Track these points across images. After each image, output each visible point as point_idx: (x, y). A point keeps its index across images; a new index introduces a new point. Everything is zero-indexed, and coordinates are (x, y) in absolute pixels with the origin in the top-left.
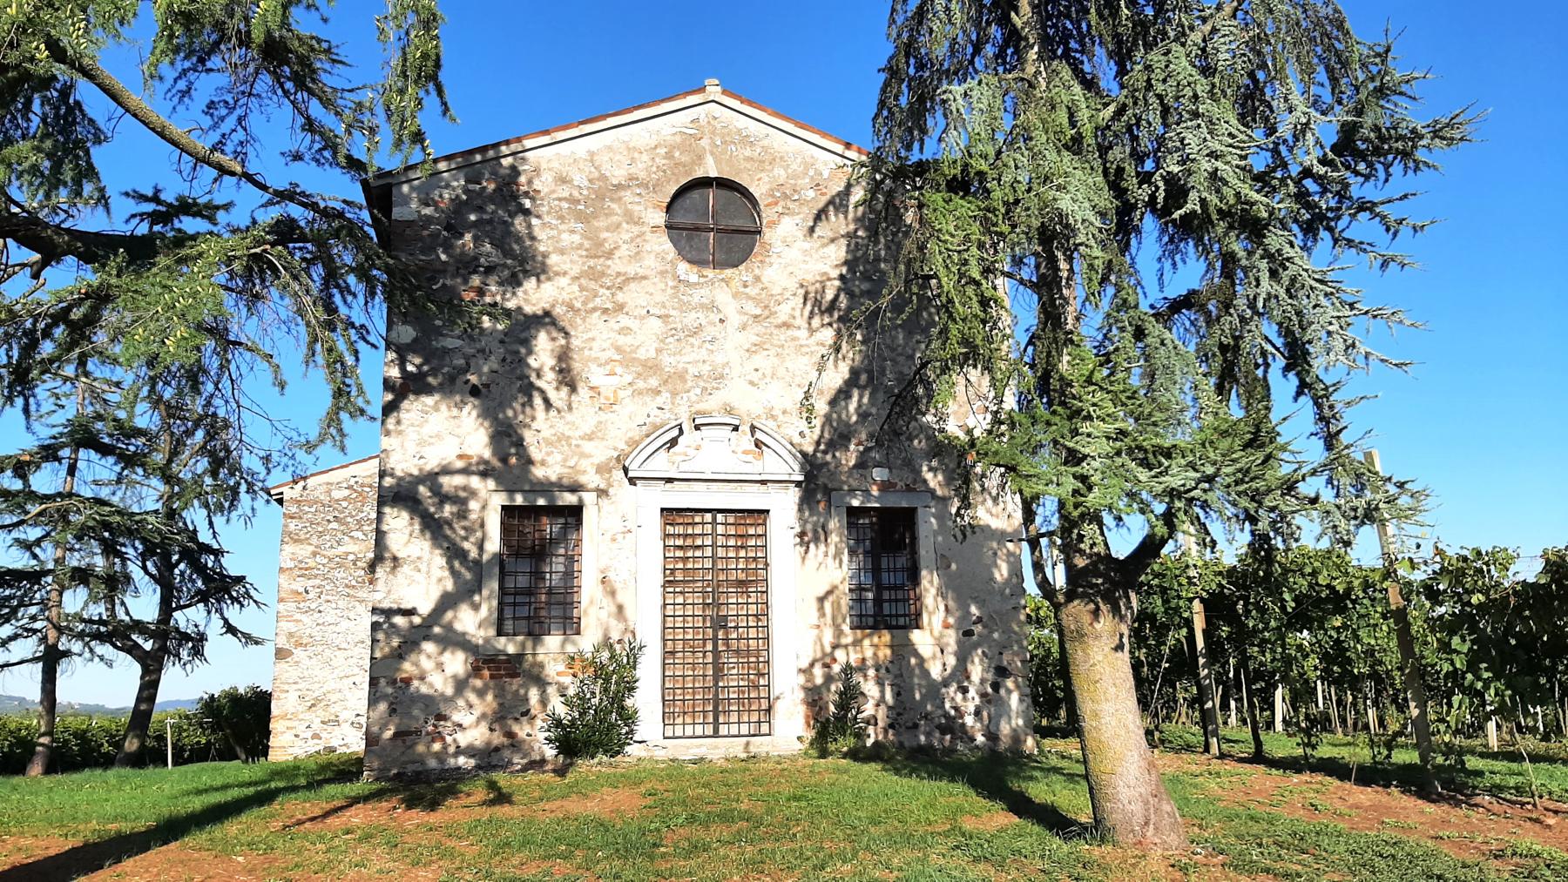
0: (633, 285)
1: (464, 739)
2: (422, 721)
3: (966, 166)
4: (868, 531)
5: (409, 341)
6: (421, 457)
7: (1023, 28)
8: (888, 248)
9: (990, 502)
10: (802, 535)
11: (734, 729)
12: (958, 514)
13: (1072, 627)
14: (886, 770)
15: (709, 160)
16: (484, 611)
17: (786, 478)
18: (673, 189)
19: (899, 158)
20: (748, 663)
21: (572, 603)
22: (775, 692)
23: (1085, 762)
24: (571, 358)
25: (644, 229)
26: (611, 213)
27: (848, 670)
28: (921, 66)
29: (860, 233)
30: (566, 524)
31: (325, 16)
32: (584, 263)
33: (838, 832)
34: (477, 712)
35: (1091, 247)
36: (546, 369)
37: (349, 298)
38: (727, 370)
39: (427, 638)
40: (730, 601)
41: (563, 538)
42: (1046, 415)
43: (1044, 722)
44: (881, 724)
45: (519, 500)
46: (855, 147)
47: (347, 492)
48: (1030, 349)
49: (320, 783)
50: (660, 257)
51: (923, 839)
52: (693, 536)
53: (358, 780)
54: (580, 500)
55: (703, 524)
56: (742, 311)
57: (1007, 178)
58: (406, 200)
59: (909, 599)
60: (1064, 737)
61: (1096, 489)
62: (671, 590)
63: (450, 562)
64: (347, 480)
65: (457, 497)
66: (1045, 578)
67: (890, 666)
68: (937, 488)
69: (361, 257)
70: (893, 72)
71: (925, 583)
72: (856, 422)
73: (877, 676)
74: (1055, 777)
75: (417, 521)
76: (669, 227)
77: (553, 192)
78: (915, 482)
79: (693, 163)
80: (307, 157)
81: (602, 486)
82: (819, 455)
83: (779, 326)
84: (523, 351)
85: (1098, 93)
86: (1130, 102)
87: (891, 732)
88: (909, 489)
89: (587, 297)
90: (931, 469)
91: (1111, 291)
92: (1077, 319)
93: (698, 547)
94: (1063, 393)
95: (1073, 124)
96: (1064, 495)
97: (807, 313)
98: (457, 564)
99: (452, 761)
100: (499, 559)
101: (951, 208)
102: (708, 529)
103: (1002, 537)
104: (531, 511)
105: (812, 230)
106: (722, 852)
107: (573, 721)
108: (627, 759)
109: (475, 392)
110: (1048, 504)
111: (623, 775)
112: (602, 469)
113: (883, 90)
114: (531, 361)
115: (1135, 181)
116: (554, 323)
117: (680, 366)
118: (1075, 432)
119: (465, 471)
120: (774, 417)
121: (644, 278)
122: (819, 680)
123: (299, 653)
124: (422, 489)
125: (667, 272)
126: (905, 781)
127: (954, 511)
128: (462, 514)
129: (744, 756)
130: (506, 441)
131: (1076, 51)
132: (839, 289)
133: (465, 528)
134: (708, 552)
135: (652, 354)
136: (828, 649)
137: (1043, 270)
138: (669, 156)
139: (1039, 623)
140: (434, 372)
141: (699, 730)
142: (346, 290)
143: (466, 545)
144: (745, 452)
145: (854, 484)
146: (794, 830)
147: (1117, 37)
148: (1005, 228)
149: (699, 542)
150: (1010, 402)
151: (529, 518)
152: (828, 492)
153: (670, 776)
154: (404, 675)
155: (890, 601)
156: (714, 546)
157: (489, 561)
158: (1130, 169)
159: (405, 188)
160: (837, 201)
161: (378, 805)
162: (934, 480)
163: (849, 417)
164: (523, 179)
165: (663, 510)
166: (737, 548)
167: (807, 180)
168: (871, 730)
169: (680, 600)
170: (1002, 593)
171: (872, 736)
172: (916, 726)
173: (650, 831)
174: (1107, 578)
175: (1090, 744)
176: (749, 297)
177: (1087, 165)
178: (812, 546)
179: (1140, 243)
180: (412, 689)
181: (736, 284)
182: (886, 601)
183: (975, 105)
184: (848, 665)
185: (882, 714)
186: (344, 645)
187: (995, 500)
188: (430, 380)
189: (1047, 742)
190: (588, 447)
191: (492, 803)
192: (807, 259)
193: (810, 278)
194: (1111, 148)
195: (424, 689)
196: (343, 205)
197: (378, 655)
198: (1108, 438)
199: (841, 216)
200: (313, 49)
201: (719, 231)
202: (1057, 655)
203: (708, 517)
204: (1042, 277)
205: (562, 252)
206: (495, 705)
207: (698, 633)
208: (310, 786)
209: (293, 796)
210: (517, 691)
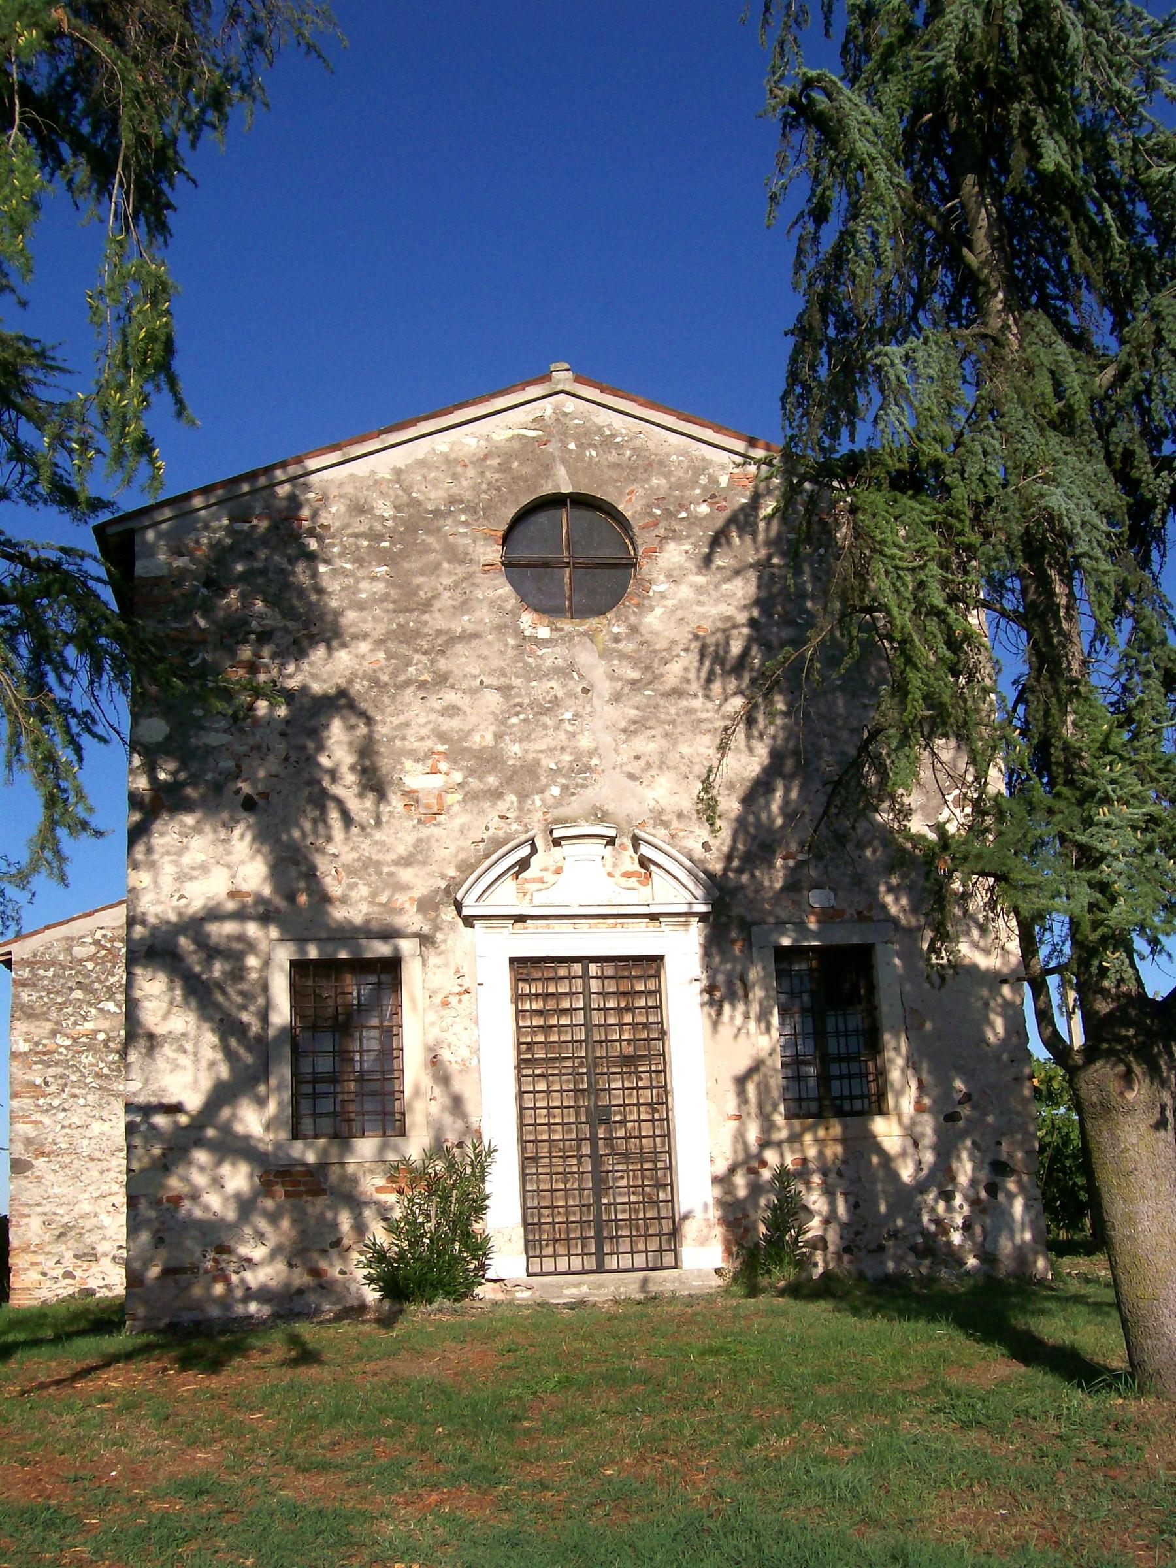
0: (459, 648)
1: (255, 1278)
2: (198, 1254)
3: (914, 459)
4: (806, 979)
5: (160, 739)
6: (182, 897)
7: (980, 269)
8: (816, 578)
9: (975, 933)
10: (710, 989)
11: (626, 1261)
12: (932, 948)
13: (1095, 1099)
14: (839, 1311)
15: (561, 471)
16: (272, 1107)
17: (684, 909)
18: (511, 512)
19: (822, 449)
20: (642, 1170)
21: (393, 1093)
22: (683, 1206)
23: (1116, 1284)
24: (377, 753)
25: (473, 568)
26: (426, 550)
27: (783, 1175)
28: (844, 325)
29: (775, 560)
30: (379, 983)
31: (24, 296)
32: (391, 621)
33: (771, 1396)
34: (273, 1238)
35: (1097, 560)
36: (344, 769)
37: (68, 678)
38: (595, 761)
39: (200, 1143)
40: (613, 1086)
41: (374, 1004)
42: (1048, 800)
43: (1063, 1235)
44: (832, 1248)
45: (313, 953)
46: (761, 443)
47: (93, 949)
48: (1021, 709)
49: (70, 1336)
50: (496, 605)
51: (891, 1401)
52: (557, 996)
53: (119, 1332)
54: (396, 949)
55: (570, 978)
56: (612, 676)
57: (973, 469)
58: (151, 551)
59: (868, 1074)
60: (1089, 1253)
61: (1121, 901)
62: (530, 1072)
63: (223, 1039)
64: (93, 933)
65: (230, 950)
66: (1055, 1032)
67: (843, 1168)
68: (901, 915)
69: (83, 622)
70: (803, 332)
71: (889, 1054)
72: (783, 827)
73: (824, 1182)
74: (1075, 1309)
75: (178, 984)
76: (509, 564)
77: (347, 525)
78: (870, 907)
79: (538, 475)
80: (15, 495)
81: (426, 929)
82: (731, 875)
83: (666, 695)
84: (311, 745)
85: (1090, 352)
86: (1134, 361)
87: (846, 1258)
88: (862, 917)
89: (396, 668)
90: (891, 889)
91: (1127, 624)
92: (1084, 663)
93: (564, 1012)
94: (1069, 770)
95: (1059, 394)
96: (1077, 911)
97: (703, 675)
98: (233, 1043)
99: (239, 1309)
100: (290, 1034)
101: (898, 512)
102: (578, 985)
103: (997, 979)
104: (328, 968)
105: (708, 560)
106: (609, 1425)
107: (401, 1255)
108: (477, 1304)
109: (249, 805)
110: (1056, 926)
111: (471, 1325)
112: (427, 905)
113: (793, 360)
114: (324, 761)
115: (1150, 468)
116: (352, 706)
117: (531, 756)
118: (1088, 822)
119: (240, 915)
120: (666, 824)
121: (476, 635)
122: (742, 1193)
123: (40, 1163)
124: (183, 941)
125: (506, 626)
126: (867, 1323)
127: (925, 946)
128: (238, 973)
129: (640, 1296)
130: (293, 872)
131: (1056, 298)
132: (750, 640)
133: (242, 993)
134: (580, 1018)
135: (489, 740)
136: (754, 1149)
137: (1031, 596)
138: (504, 468)
139: (1051, 1098)
140: (194, 781)
141: (577, 1263)
142: (62, 666)
143: (245, 1017)
144: (627, 875)
145: (784, 915)
146: (711, 1394)
147: (1111, 278)
148: (975, 538)
149: (565, 1005)
150: (997, 782)
151: (328, 977)
152: (746, 926)
153: (535, 1326)
154: (171, 1194)
155: (841, 1077)
156: (587, 1009)
157: (277, 1038)
158: (1142, 452)
159: (150, 535)
160: (741, 517)
161: (143, 1365)
162: (895, 905)
163: (771, 820)
164: (305, 512)
165: (512, 960)
166: (620, 1011)
167: (698, 491)
168: (819, 1257)
169: (542, 1086)
170: (998, 1059)
171: (820, 1264)
172: (881, 1249)
173: (510, 1400)
174: (1141, 1029)
175: (1124, 1259)
176: (622, 656)
177: (1082, 449)
178: (727, 1008)
179: (1163, 556)
180: (183, 1211)
181: (603, 636)
182: (835, 1078)
183: (921, 370)
184: (783, 1167)
185: (832, 1236)
186: (97, 1154)
187: (983, 930)
188: (189, 791)
189: (1066, 1260)
190: (406, 875)
191: (295, 1363)
192: (702, 598)
193: (707, 624)
194: (1113, 424)
195: (198, 1213)
196: (60, 554)
197: (135, 1166)
198: (1135, 828)
199: (748, 539)
200: (20, 353)
201: (577, 566)
202: (1077, 1143)
203: (577, 968)
204: (1031, 606)
205: (361, 606)
206: (293, 1233)
207: (570, 1131)
208: (57, 1340)
209: (35, 1351)
210: (322, 1214)
